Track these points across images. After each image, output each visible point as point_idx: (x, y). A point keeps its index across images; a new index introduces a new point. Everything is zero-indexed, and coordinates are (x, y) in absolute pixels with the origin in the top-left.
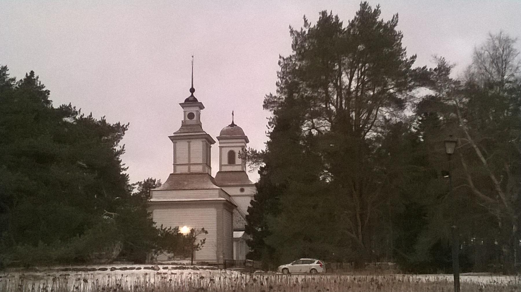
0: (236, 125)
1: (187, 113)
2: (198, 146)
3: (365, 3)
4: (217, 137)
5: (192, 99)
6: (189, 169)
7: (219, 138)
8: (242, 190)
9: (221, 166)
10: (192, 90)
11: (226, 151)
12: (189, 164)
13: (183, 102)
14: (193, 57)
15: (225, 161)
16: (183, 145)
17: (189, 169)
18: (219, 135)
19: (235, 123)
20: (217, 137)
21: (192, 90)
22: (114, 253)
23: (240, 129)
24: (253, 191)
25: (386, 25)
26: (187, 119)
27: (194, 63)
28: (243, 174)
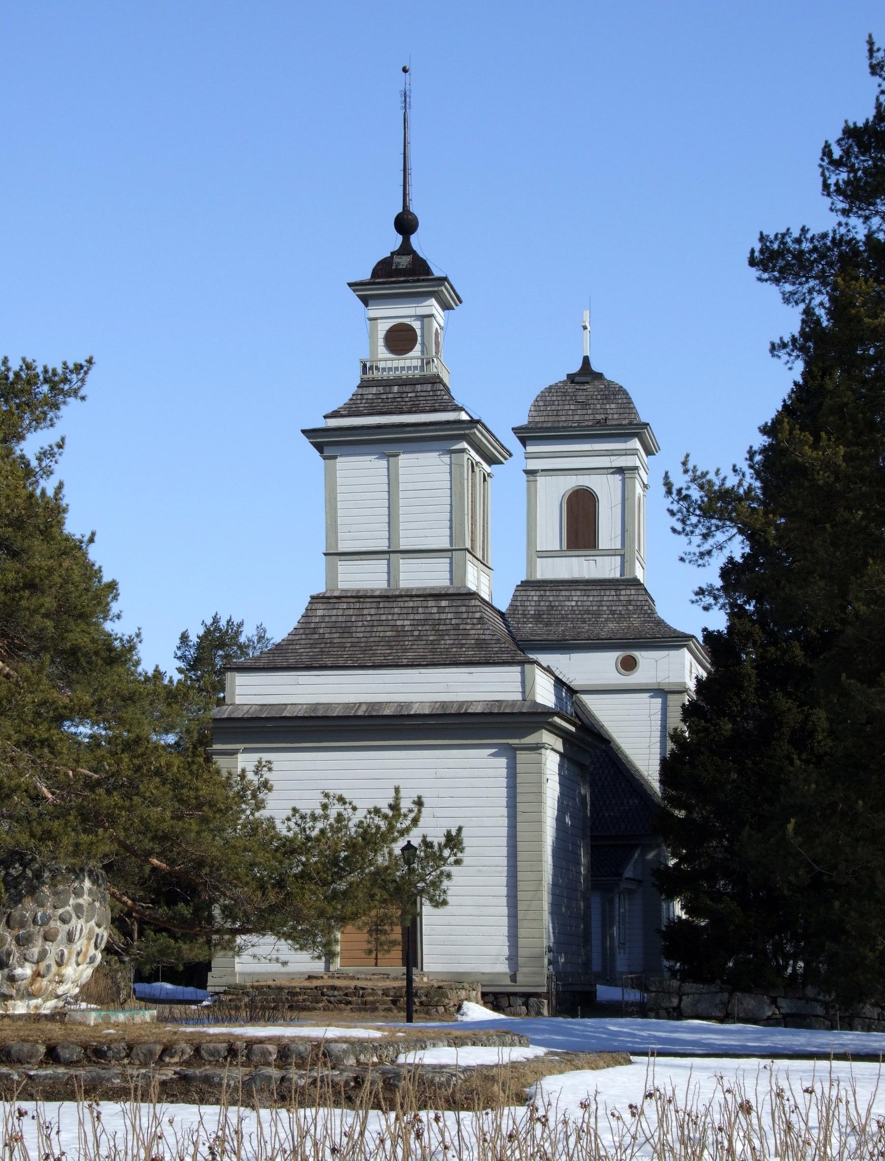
0: (600, 376)
1: (383, 327)
2: (425, 472)
3: (752, 262)
4: (516, 430)
5: (404, 261)
6: (392, 574)
7: (525, 435)
8: (629, 665)
9: (536, 554)
10: (405, 224)
11: (552, 494)
12: (391, 553)
13: (367, 276)
14: (405, 70)
15: (551, 530)
16: (361, 472)
17: (392, 574)
18: (523, 421)
19: (596, 367)
20: (516, 430)
21: (405, 224)
22: (69, 971)
23: (616, 394)
24: (687, 669)
25: (802, 333)
26: (383, 352)
27: (414, 100)
28: (626, 594)
